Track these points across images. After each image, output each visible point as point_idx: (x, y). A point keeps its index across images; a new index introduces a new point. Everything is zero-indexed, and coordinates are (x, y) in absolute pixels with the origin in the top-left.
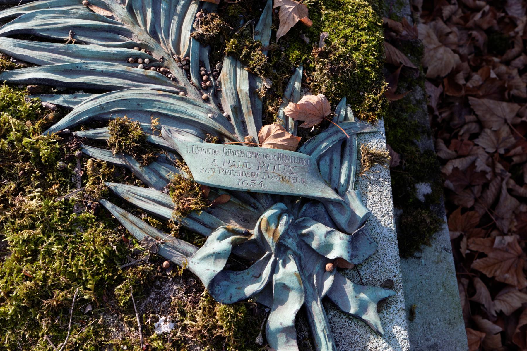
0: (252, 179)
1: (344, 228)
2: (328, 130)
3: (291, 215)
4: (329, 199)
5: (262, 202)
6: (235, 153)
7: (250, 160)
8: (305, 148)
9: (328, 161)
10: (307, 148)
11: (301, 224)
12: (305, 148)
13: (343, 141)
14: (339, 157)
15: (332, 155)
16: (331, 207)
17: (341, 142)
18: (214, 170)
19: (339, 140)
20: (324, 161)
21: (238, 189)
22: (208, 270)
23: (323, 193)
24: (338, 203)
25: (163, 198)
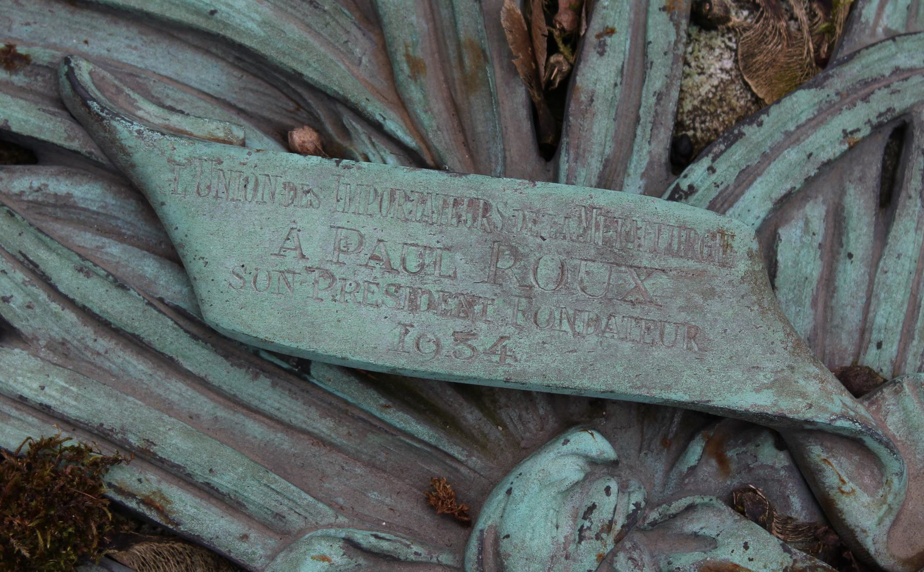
0: (459, 325)
1: (872, 550)
2: (827, 77)
3: (634, 483)
4: (807, 422)
5: (507, 421)
6: (385, 204)
7: (458, 234)
8: (711, 170)
9: (818, 226)
10: (722, 167)
11: (678, 523)
12: (711, 170)
13: (895, 125)
14: (872, 204)
15: (843, 193)
16: (817, 452)
17: (888, 131)
18: (290, 277)
19: (877, 128)
20: (801, 224)
21: (394, 369)
22: (367, 99)
23: (779, 394)
24: (847, 438)
25: (64, 391)
